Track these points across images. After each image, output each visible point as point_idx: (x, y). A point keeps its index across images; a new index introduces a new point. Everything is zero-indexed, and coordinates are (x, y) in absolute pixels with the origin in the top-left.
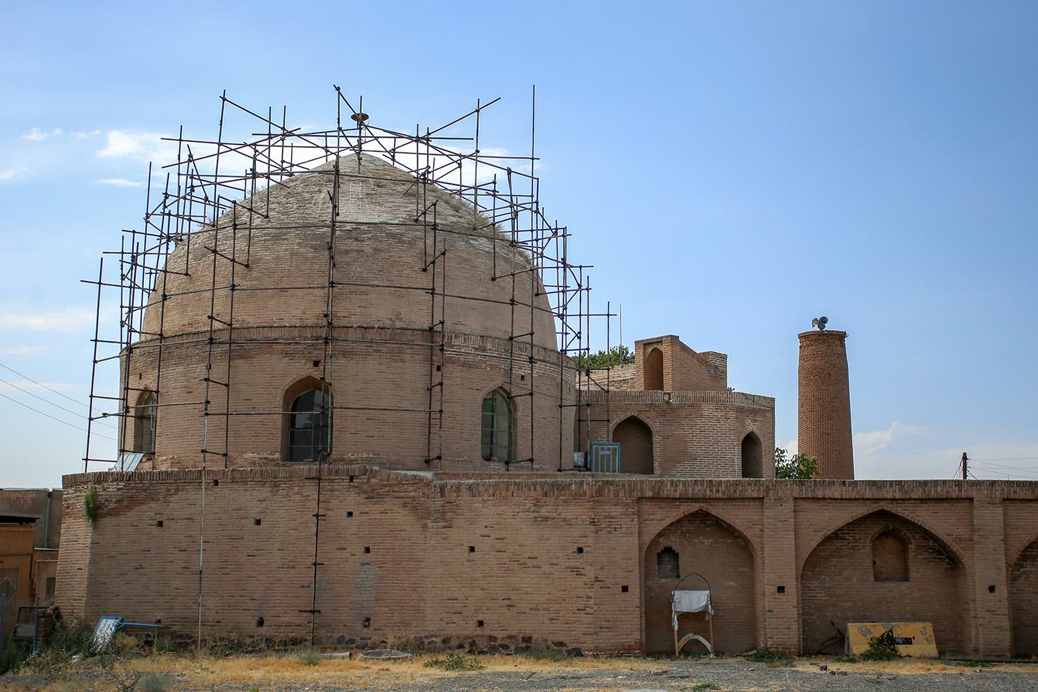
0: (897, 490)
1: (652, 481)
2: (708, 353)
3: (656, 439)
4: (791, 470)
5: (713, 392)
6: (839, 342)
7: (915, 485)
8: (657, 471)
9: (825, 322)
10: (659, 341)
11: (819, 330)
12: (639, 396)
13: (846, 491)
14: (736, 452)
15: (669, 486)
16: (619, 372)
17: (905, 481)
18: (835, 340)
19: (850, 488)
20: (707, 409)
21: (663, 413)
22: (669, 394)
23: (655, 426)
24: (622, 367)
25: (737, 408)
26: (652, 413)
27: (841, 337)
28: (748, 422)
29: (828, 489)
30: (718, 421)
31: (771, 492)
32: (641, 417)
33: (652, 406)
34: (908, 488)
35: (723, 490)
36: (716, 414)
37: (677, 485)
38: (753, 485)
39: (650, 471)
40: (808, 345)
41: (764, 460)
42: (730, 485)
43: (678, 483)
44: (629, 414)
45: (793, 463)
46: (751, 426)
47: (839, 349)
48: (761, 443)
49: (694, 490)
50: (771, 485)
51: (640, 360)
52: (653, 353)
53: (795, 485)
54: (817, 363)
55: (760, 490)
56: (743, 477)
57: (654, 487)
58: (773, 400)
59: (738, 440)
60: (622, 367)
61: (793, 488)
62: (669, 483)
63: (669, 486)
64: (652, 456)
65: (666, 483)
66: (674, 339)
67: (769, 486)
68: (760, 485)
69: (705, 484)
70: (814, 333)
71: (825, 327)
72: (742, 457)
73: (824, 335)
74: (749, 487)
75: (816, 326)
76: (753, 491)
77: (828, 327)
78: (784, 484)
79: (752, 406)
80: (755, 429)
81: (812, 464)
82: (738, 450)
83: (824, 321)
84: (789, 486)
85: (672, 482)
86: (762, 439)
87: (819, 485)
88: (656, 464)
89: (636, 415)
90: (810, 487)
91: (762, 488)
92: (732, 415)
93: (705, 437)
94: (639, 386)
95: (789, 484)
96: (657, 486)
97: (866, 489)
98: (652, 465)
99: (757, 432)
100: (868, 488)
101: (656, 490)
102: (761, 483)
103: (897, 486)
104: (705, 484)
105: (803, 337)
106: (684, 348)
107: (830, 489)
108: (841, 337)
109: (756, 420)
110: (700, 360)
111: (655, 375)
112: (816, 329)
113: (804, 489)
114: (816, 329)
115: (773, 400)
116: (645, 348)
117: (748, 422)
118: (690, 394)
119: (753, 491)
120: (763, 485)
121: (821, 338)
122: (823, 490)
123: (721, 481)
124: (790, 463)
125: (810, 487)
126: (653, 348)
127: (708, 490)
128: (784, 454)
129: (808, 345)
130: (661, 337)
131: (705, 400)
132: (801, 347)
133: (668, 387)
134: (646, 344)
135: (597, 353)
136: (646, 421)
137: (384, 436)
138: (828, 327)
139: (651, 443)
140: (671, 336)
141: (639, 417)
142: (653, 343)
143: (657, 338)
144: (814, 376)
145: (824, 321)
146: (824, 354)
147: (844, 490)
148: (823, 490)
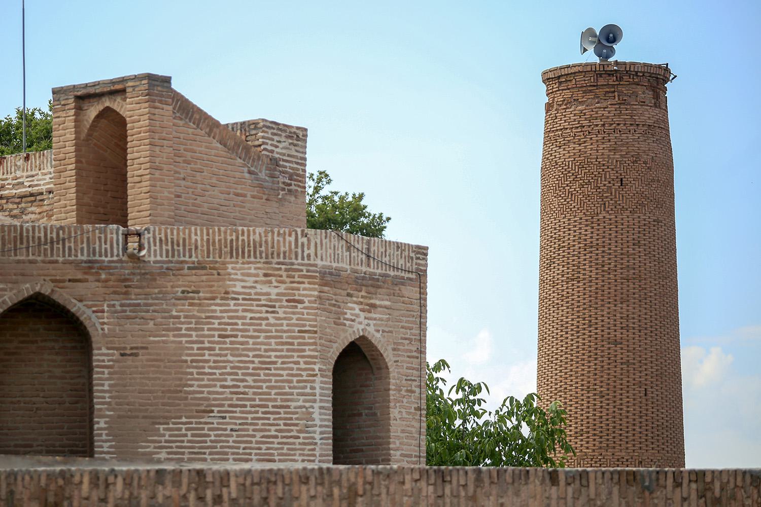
0: (694, 496)
1: (39, 475)
2: (255, 124)
3: (102, 355)
4: (503, 438)
5: (258, 230)
6: (649, 94)
7: (739, 483)
8: (103, 443)
9: (614, 40)
10: (117, 89)
11: (597, 60)
12: (57, 239)
13: (559, 498)
14: (318, 391)
15: (86, 486)
16: (19, 174)
17: (713, 472)
18: (639, 90)
19: (570, 490)
20: (243, 277)
21: (123, 286)
22: (139, 235)
23: (100, 321)
24: (27, 158)
25: (323, 274)
26: (92, 287)
27: (656, 79)
28: (353, 309)
29: (510, 493)
30: (271, 308)
31: (360, 499)
32: (65, 297)
33: (91, 267)
34: (722, 489)
35: (234, 495)
36: (265, 289)
37: (107, 485)
38: (312, 481)
39: (84, 447)
40: (567, 103)
41: (394, 413)
42: (253, 484)
43: (111, 479)
44: (27, 289)
45: (502, 419)
46: (360, 323)
47: (648, 115)
48: (387, 368)
49: (153, 497)
50: (360, 481)
51: (65, 136)
52: (103, 122)
53: (423, 484)
54: (589, 148)
55: (331, 495)
56: (334, 464)
57: (45, 490)
58: (422, 252)
59: (323, 359)
60: (27, 158)
61: (420, 490)
62: (86, 480)
63: (86, 486)
64: (91, 407)
65: (77, 479)
66: (158, 86)
67: (354, 484)
68: (331, 483)
69: (185, 481)
70: (585, 70)
71: (612, 52)
72: (334, 405)
73: (610, 74)
74: (304, 488)
75: (591, 50)
76: (313, 497)
77: (622, 53)
78: (397, 478)
79: (364, 269)
80: (371, 329)
81: (553, 423)
82: (322, 387)
83: (609, 37)
84: (408, 486)
85: (95, 477)
86: (389, 357)
87: (487, 480)
88: (100, 424)
89: (46, 290)
90: (465, 486)
91: (336, 491)
92: (308, 291)
93: (235, 352)
94: (63, 213)
95: (408, 478)
96: (52, 487)
97: (610, 493)
98: (91, 429)
99: (376, 337)
100: (615, 490)
101: (51, 499)
102: (335, 477)
103: (694, 486)
104: (185, 481)
105: (557, 79)
106: (186, 110)
107: (517, 494)
108: (656, 79)
109: (373, 306)
110: (231, 143)
111: (105, 185)
112: (591, 57)
113: (448, 491)
114: (591, 57)
115: (422, 252)
116: (79, 109)
117: (353, 309)
118: (197, 236)
119: (313, 497)
120: (339, 483)
121: (601, 81)
122: (500, 496)
123: (228, 473)
124: (493, 419)
125: (465, 486)
126: (101, 108)
127: (192, 497)
128: (479, 396)
129: (567, 103)
130: (123, 80)
131: (237, 251)
132: (549, 107)
133: (137, 218)
134: (83, 97)
135: (14, 116)
136: (76, 307)
137: (122, 355)
138: (622, 53)
139: (90, 370)
140: (151, 78)
141: (55, 297)
142: (99, 96)
143: (113, 82)
144: (582, 186)
145: (609, 37)
146: (611, 127)
147: (554, 496)
148: (500, 496)
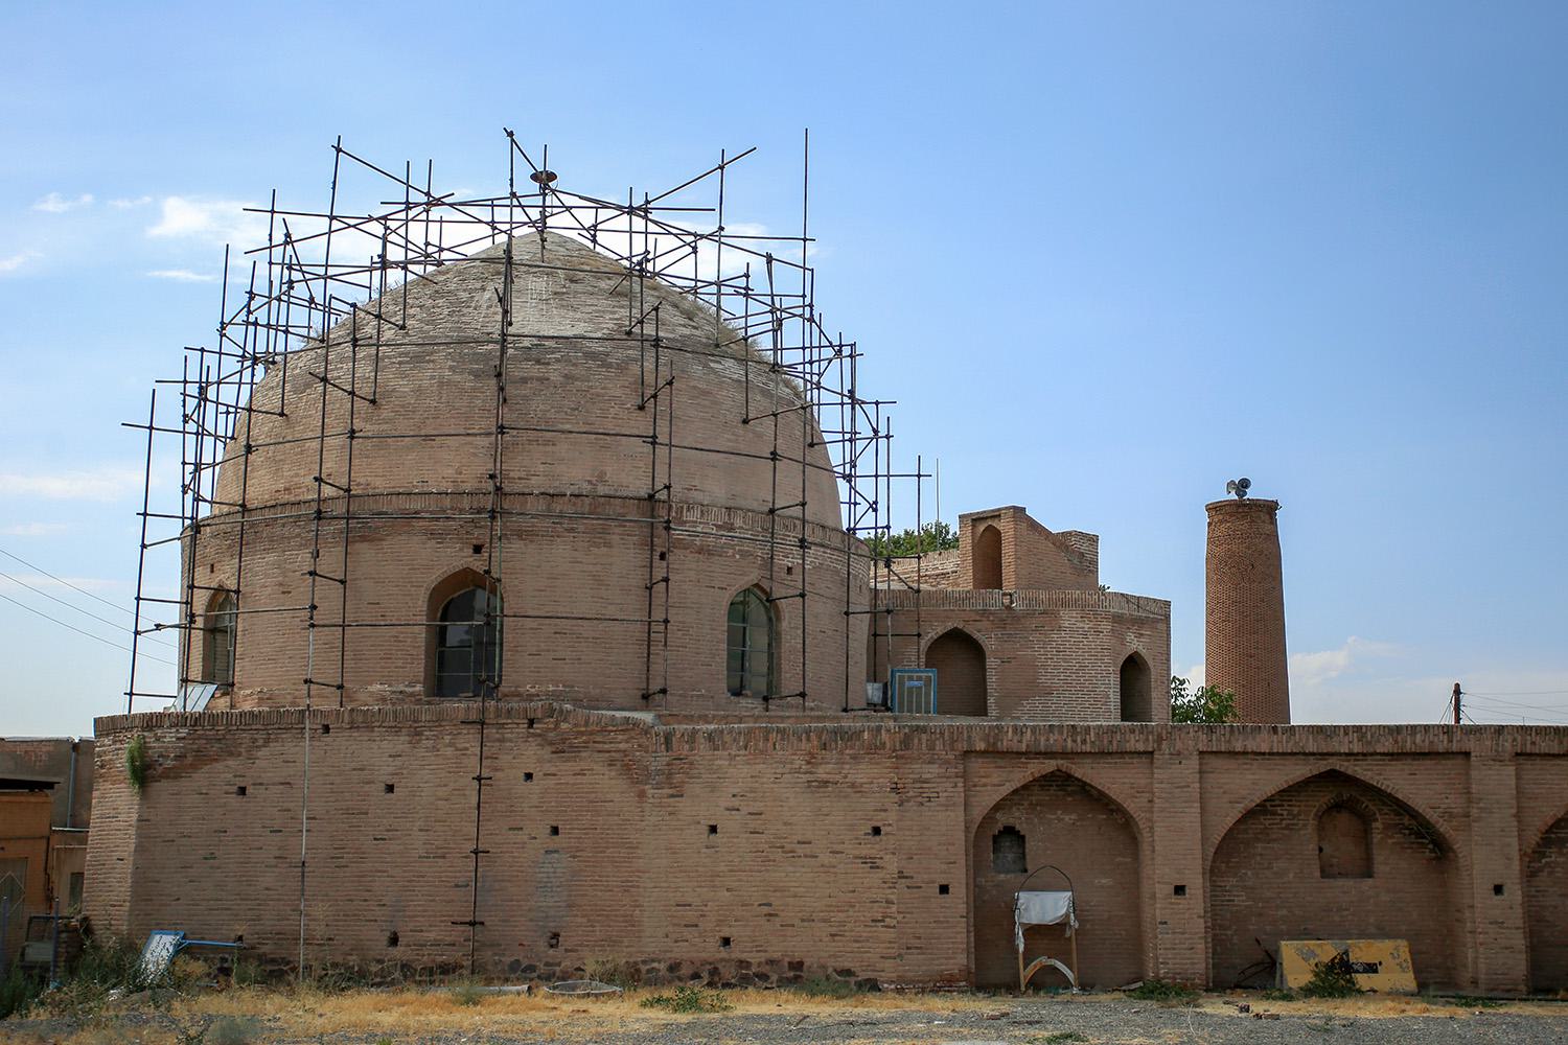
0: (1356, 740)
1: (985, 727)
2: (1070, 533)
3: (991, 662)
4: (1195, 709)
5: (1078, 592)
6: (1268, 516)
7: (1382, 732)
8: (993, 711)
9: (1247, 487)
10: (996, 515)
11: (1236, 498)
12: (966, 597)
13: (1279, 742)
14: (1112, 682)
15: (1010, 733)
16: (935, 562)
17: (1366, 726)
18: (1262, 514)
19: (1284, 737)
20: (1069, 618)
21: (1002, 624)
22: (1010, 595)
23: (989, 643)
24: (940, 554)
25: (1114, 617)
26: (985, 624)
27: (1270, 508)
28: (1130, 637)
29: (1250, 738)
30: (1085, 636)
31: (1164, 742)
32: (969, 629)
33: (985, 613)
34: (1372, 737)
35: (1093, 739)
36: (1082, 625)
37: (1022, 733)
38: (1137, 732)
39: (982, 711)
40: (1221, 522)
41: (1154, 695)
42: (1103, 733)
43: (1024, 730)
44: (950, 626)
45: (1198, 698)
46: (1134, 644)
47: (1268, 527)
48: (1149, 669)
49: (1048, 740)
50: (1164, 732)
51: (966, 543)
52: (987, 533)
53: (1200, 733)
54: (1234, 548)
55: (1147, 740)
56: (1122, 720)
57: (988, 735)
58: (1168, 604)
59: (1115, 665)
60: (940, 554)
61: (1198, 737)
62: (1010, 730)
63: (1010, 733)
64: (986, 689)
65: (1006, 729)
66: (1018, 512)
67: (1161, 733)
68: (1148, 733)
69: (1065, 731)
70: (1230, 503)
71: (1246, 493)
72: (1121, 690)
73: (1245, 505)
74: (1132, 736)
75: (1233, 492)
76: (1137, 741)
77: (1251, 494)
78: (1185, 730)
79: (1136, 613)
80: (1141, 648)
81: (1227, 701)
82: (1114, 680)
83: (1244, 484)
84: (1191, 735)
85: (1015, 728)
86: (1151, 663)
87: (1236, 733)
88: (991, 701)
89: (960, 627)
90: (1224, 735)
91: (1150, 737)
92: (1106, 626)
93: (1065, 661)
94: (966, 583)
95: (1191, 730)
96: (992, 734)
97: (1308, 739)
98: (986, 703)
99: (1144, 652)
100: (1311, 737)
101: (992, 740)
102: (1150, 729)
103: (1355, 735)
104: (1065, 731)
105: (1214, 509)
106: (1034, 526)
107: (1254, 739)
108: (1270, 508)
109: (1142, 634)
110: (1058, 544)
111: (989, 567)
112: (1233, 496)
113: (1214, 738)
114: (1233, 496)
115: (1168, 604)
116: (974, 526)
117: (1130, 637)
118: (1043, 595)
119: (1137, 741)
120: (1152, 732)
121: (1240, 510)
122: (1244, 741)
123: (1089, 727)
124: (1194, 699)
125: (1224, 735)
126: (986, 525)
127: (1069, 740)
128: (1184, 686)
129: (1221, 522)
130: (999, 510)
131: (1065, 604)
132: (1210, 524)
133: (1009, 584)
134: (976, 519)
135: (902, 534)
136: (976, 635)
137: (579, 659)
138: (1251, 494)
139: (984, 669)
140: (1014, 507)
141: (965, 630)
142: (987, 518)
143: (993, 511)
144: (1230, 569)
145: (1244, 484)
146: (1245, 535)
147: (1275, 740)
148: (1244, 741)
